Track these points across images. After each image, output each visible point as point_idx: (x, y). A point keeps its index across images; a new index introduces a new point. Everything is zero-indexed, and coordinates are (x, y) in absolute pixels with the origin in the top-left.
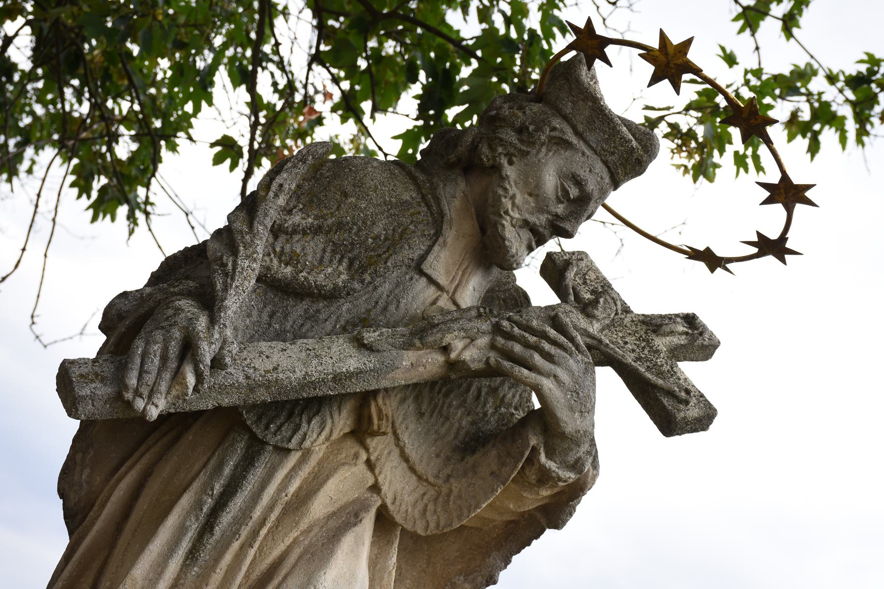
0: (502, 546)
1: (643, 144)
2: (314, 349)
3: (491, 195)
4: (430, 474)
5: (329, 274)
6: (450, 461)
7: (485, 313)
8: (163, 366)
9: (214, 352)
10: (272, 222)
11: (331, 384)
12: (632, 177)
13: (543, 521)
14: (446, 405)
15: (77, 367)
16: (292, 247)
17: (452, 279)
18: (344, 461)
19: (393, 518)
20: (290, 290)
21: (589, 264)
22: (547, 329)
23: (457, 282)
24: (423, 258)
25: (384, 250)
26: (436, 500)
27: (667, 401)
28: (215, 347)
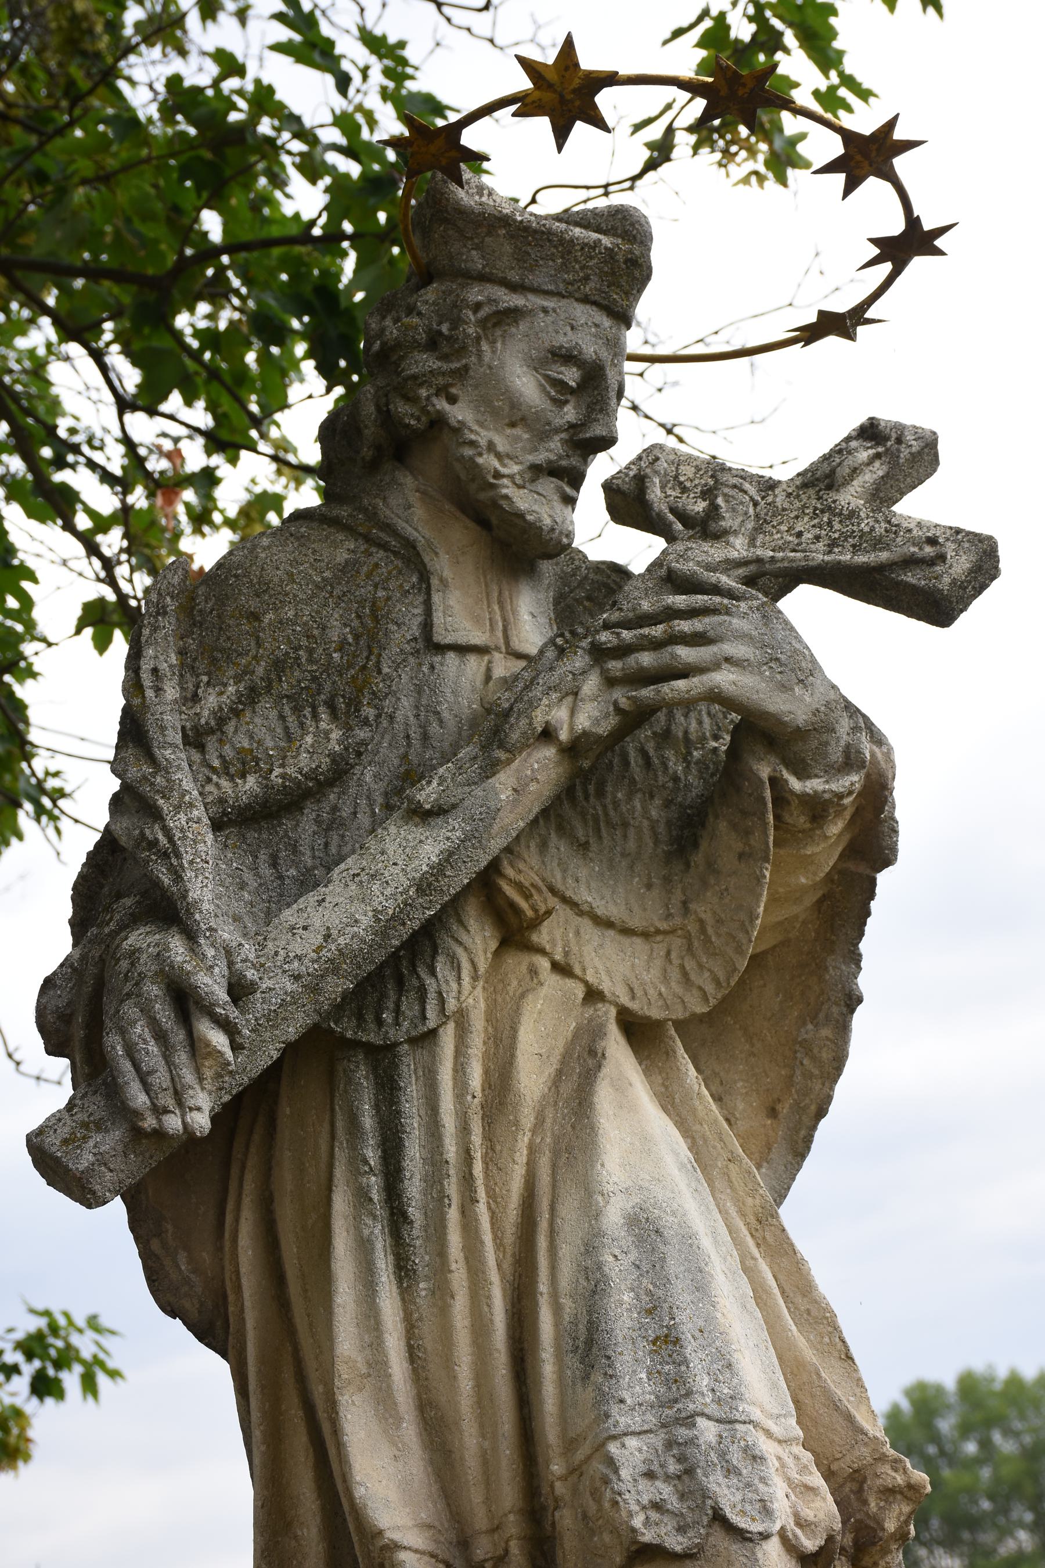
0: (833, 942)
1: (619, 232)
2: (363, 869)
3: (458, 466)
4: (655, 918)
5: (312, 746)
6: (671, 881)
7: (567, 642)
8: (167, 1049)
9: (224, 976)
10: (179, 731)
11: (421, 900)
12: (640, 291)
13: (863, 869)
14: (610, 807)
15: (51, 1133)
16: (233, 746)
17: (491, 625)
18: (520, 991)
19: (649, 1018)
20: (274, 808)
21: (672, 457)
22: (669, 601)
23: (500, 624)
24: (427, 626)
25: (365, 654)
26: (690, 949)
27: (913, 575)
28: (221, 969)
